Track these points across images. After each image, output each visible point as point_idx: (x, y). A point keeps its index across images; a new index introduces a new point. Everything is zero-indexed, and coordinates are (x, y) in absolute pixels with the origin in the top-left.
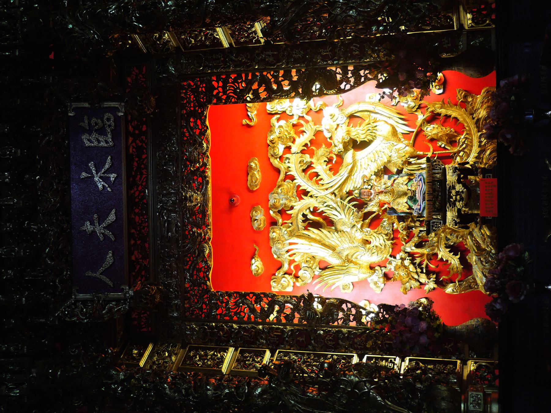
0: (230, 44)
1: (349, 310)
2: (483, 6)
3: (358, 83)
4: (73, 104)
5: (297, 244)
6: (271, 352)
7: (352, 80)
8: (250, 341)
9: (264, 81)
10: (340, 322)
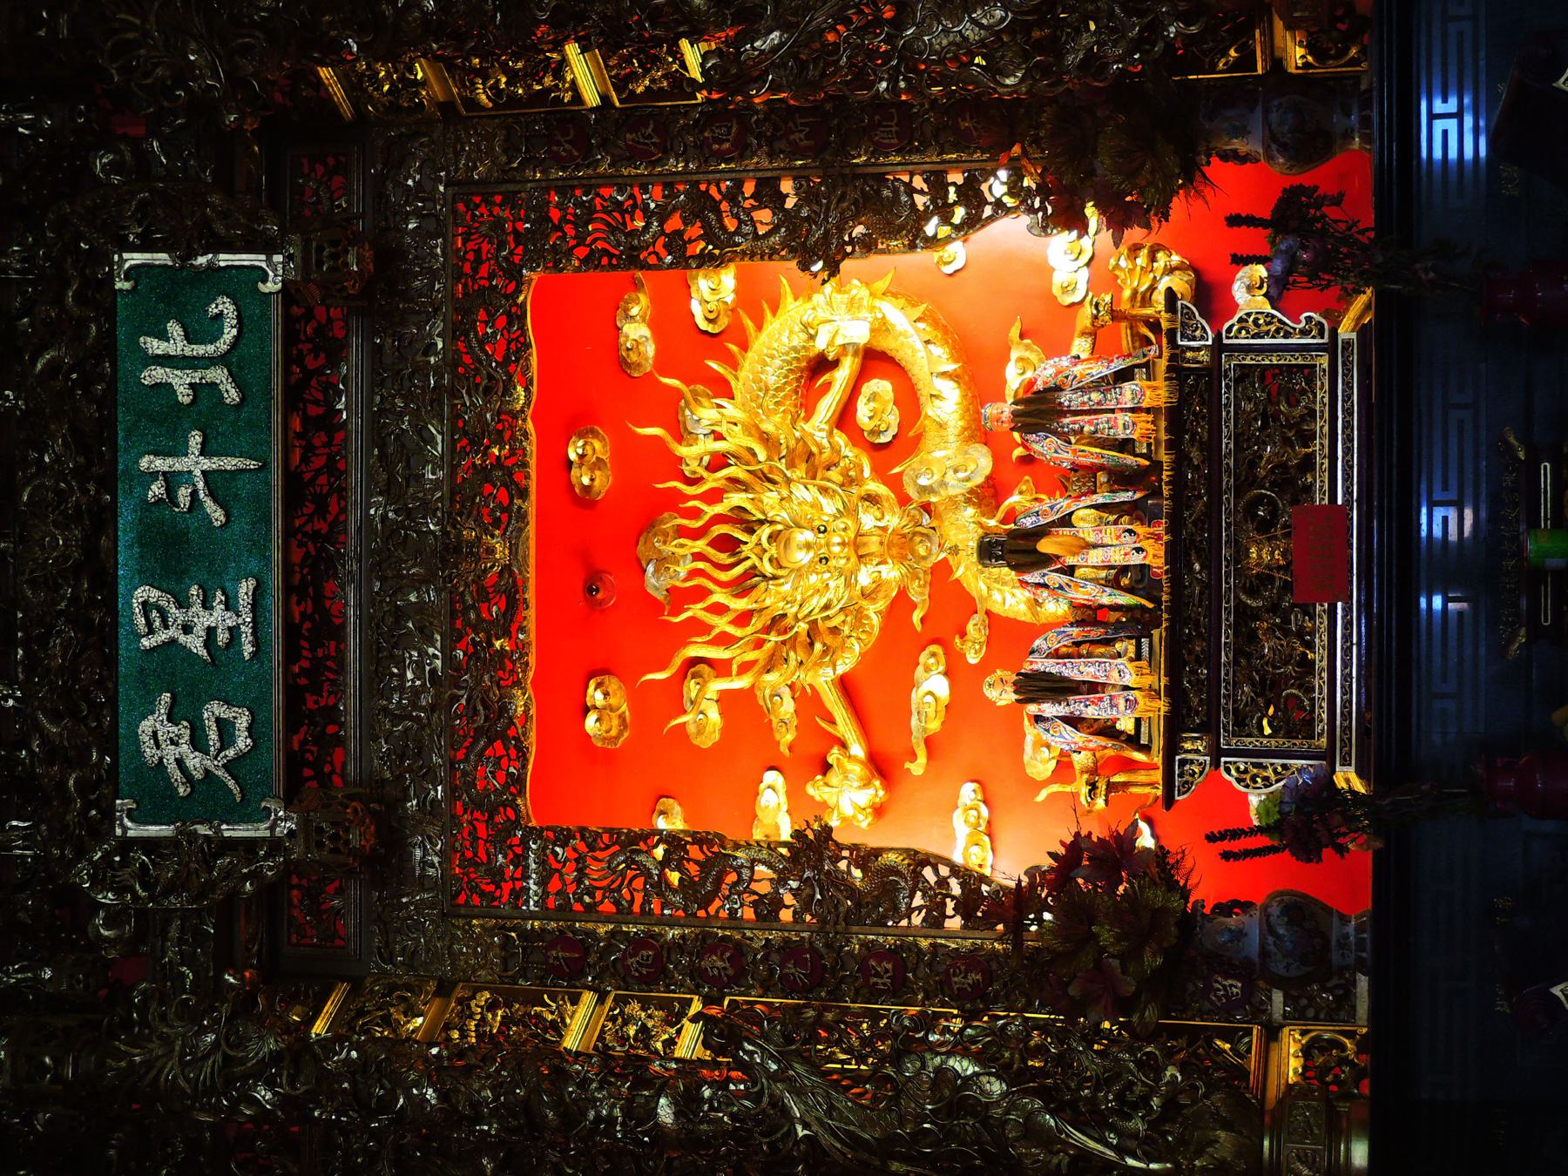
0: (605, 98)
1: (942, 882)
2: (1340, 13)
4: (125, 256)
8: (642, 970)
9: (701, 207)
10: (917, 920)
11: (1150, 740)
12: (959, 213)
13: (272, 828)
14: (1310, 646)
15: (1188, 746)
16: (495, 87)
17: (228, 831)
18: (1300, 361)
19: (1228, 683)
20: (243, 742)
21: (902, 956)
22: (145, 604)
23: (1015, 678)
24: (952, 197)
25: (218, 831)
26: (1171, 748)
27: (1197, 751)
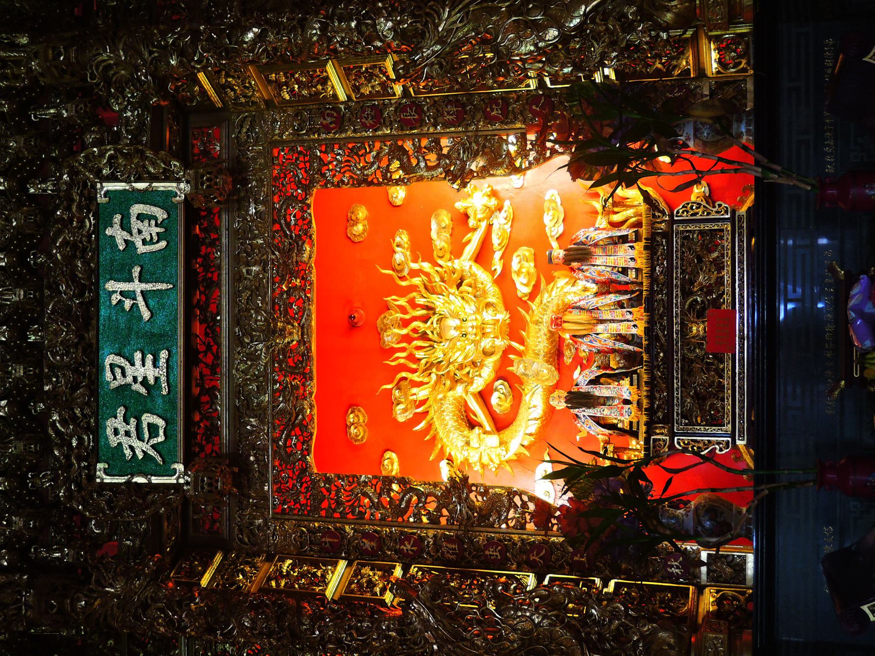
0: (349, 97)
1: (524, 505)
3: (541, 158)
4: (104, 184)
5: (144, 365)
6: (403, 569)
7: (532, 155)
8: (369, 552)
9: (398, 152)
11: (638, 428)
12: (532, 155)
13: (177, 479)
14: (722, 377)
15: (658, 431)
16: (293, 90)
17: (155, 480)
18: (716, 227)
19: (678, 398)
20: (161, 438)
21: (504, 545)
22: (111, 365)
23: (566, 394)
24: (529, 147)
25: (149, 480)
26: (649, 432)
27: (662, 434)
